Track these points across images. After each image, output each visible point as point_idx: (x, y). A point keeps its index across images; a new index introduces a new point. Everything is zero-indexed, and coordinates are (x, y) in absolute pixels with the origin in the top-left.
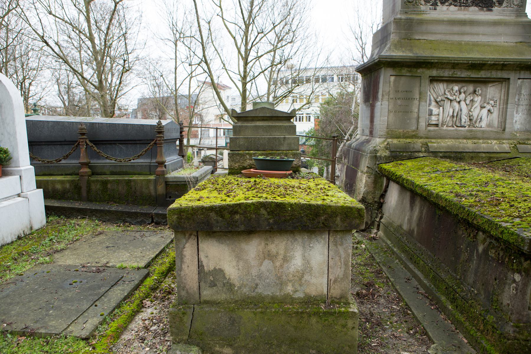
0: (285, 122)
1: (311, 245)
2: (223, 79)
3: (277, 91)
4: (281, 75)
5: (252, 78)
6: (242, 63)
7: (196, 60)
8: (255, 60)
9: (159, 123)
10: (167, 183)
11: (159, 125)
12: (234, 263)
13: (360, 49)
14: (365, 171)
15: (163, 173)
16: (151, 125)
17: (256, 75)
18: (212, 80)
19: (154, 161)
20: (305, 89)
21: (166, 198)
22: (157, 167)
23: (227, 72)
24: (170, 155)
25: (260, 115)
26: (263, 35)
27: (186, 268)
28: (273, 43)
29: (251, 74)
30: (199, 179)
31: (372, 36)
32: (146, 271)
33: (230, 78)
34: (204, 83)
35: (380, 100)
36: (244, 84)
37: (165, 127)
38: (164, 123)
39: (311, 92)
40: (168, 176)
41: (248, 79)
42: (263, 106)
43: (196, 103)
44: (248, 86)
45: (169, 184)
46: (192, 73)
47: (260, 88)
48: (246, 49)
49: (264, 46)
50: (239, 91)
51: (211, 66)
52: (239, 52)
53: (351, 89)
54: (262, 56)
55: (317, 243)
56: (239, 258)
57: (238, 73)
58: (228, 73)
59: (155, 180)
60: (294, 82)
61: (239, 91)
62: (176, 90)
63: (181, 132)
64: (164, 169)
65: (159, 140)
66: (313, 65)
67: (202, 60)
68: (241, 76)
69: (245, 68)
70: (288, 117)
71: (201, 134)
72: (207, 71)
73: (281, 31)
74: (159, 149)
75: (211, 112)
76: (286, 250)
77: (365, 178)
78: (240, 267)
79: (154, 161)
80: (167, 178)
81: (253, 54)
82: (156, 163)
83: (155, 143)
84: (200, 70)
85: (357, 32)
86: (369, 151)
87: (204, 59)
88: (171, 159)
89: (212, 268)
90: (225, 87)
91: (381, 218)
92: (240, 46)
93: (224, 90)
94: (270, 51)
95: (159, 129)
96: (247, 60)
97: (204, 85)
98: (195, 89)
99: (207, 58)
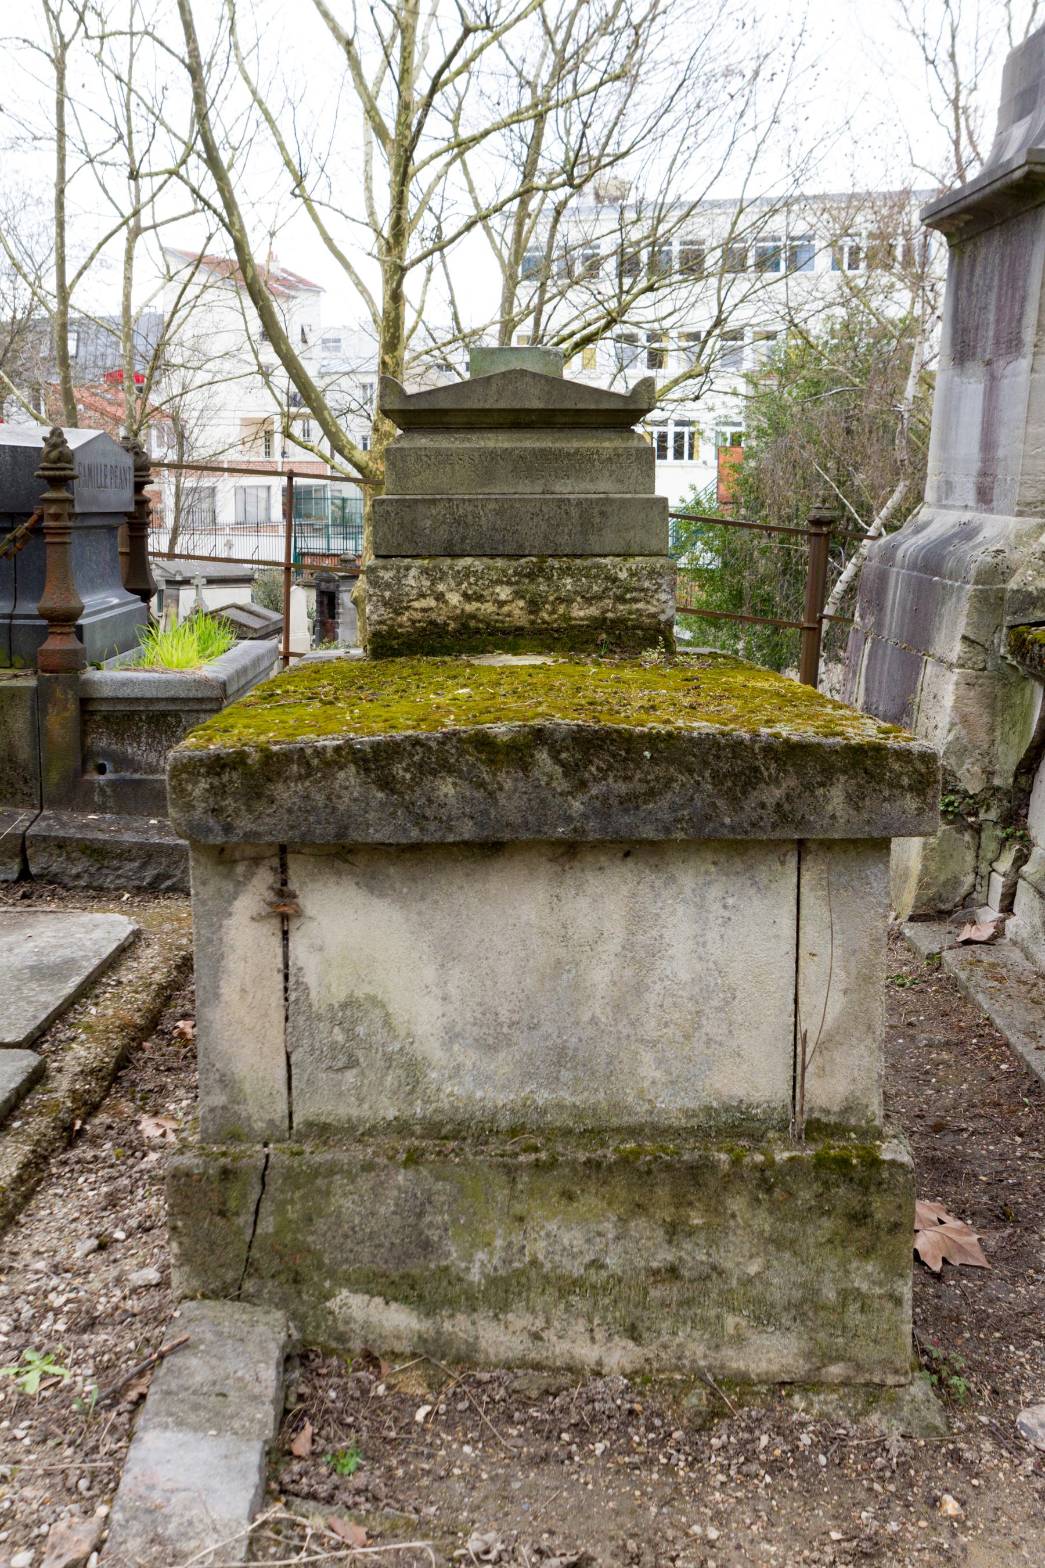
0: (607, 434)
1: (730, 901)
2: (285, 246)
3: (547, 308)
4: (570, 232)
5: (430, 245)
6: (383, 174)
7: (163, 154)
8: (446, 157)
9: (56, 441)
10: (88, 707)
11: (55, 446)
12: (430, 973)
13: (948, 116)
14: (953, 657)
15: (72, 665)
16: (14, 449)
17: (448, 233)
18: (240, 246)
19: (30, 607)
20: (682, 308)
21: (84, 771)
22: (42, 634)
23: (311, 210)
24: (93, 586)
25: (503, 405)
26: (489, 34)
27: (236, 997)
28: (529, 74)
29: (428, 221)
30: (231, 690)
31: (1007, 50)
32: (29, 1059)
33: (328, 240)
34: (199, 261)
35: (1028, 349)
36: (396, 272)
37: (78, 458)
38: (75, 439)
39: (709, 324)
40: (91, 674)
41: (413, 248)
42: (516, 365)
43: (158, 362)
44: (412, 284)
45: (93, 713)
46: (136, 213)
47: (464, 298)
48: (405, 107)
49: (489, 91)
50: (370, 302)
51: (232, 176)
52: (371, 112)
53: (899, 304)
54: (475, 140)
55: (752, 892)
56: (447, 954)
57: (363, 216)
58: (315, 218)
59: (36, 690)
60: (627, 265)
61: (370, 302)
62: (63, 293)
63: (139, 487)
64: (71, 644)
65: (56, 517)
66: (726, 190)
67: (190, 149)
68: (379, 233)
69: (400, 200)
70: (621, 414)
71: (178, 510)
72: (217, 202)
73: (573, 15)
74: (52, 554)
75: (225, 404)
76: (636, 919)
77: (951, 687)
78: (451, 989)
79: (30, 607)
80: (87, 683)
81: (436, 130)
82: (41, 616)
83: (37, 531)
84: (175, 198)
85: (933, 31)
86: (973, 573)
87: (200, 146)
88: (102, 603)
89: (339, 995)
90: (294, 285)
91: (1022, 859)
92: (379, 80)
93: (289, 298)
94: (517, 117)
95: (55, 467)
96: (409, 158)
97: (201, 278)
98: (152, 296)
99: (217, 136)
